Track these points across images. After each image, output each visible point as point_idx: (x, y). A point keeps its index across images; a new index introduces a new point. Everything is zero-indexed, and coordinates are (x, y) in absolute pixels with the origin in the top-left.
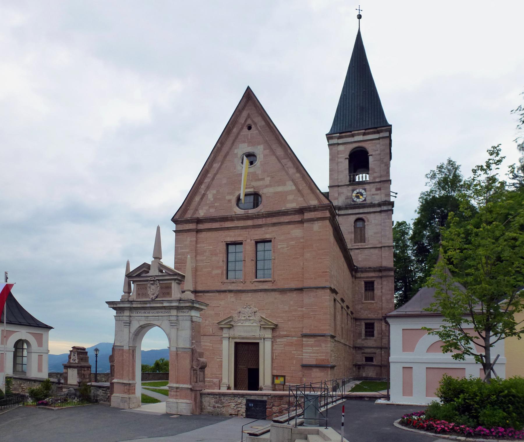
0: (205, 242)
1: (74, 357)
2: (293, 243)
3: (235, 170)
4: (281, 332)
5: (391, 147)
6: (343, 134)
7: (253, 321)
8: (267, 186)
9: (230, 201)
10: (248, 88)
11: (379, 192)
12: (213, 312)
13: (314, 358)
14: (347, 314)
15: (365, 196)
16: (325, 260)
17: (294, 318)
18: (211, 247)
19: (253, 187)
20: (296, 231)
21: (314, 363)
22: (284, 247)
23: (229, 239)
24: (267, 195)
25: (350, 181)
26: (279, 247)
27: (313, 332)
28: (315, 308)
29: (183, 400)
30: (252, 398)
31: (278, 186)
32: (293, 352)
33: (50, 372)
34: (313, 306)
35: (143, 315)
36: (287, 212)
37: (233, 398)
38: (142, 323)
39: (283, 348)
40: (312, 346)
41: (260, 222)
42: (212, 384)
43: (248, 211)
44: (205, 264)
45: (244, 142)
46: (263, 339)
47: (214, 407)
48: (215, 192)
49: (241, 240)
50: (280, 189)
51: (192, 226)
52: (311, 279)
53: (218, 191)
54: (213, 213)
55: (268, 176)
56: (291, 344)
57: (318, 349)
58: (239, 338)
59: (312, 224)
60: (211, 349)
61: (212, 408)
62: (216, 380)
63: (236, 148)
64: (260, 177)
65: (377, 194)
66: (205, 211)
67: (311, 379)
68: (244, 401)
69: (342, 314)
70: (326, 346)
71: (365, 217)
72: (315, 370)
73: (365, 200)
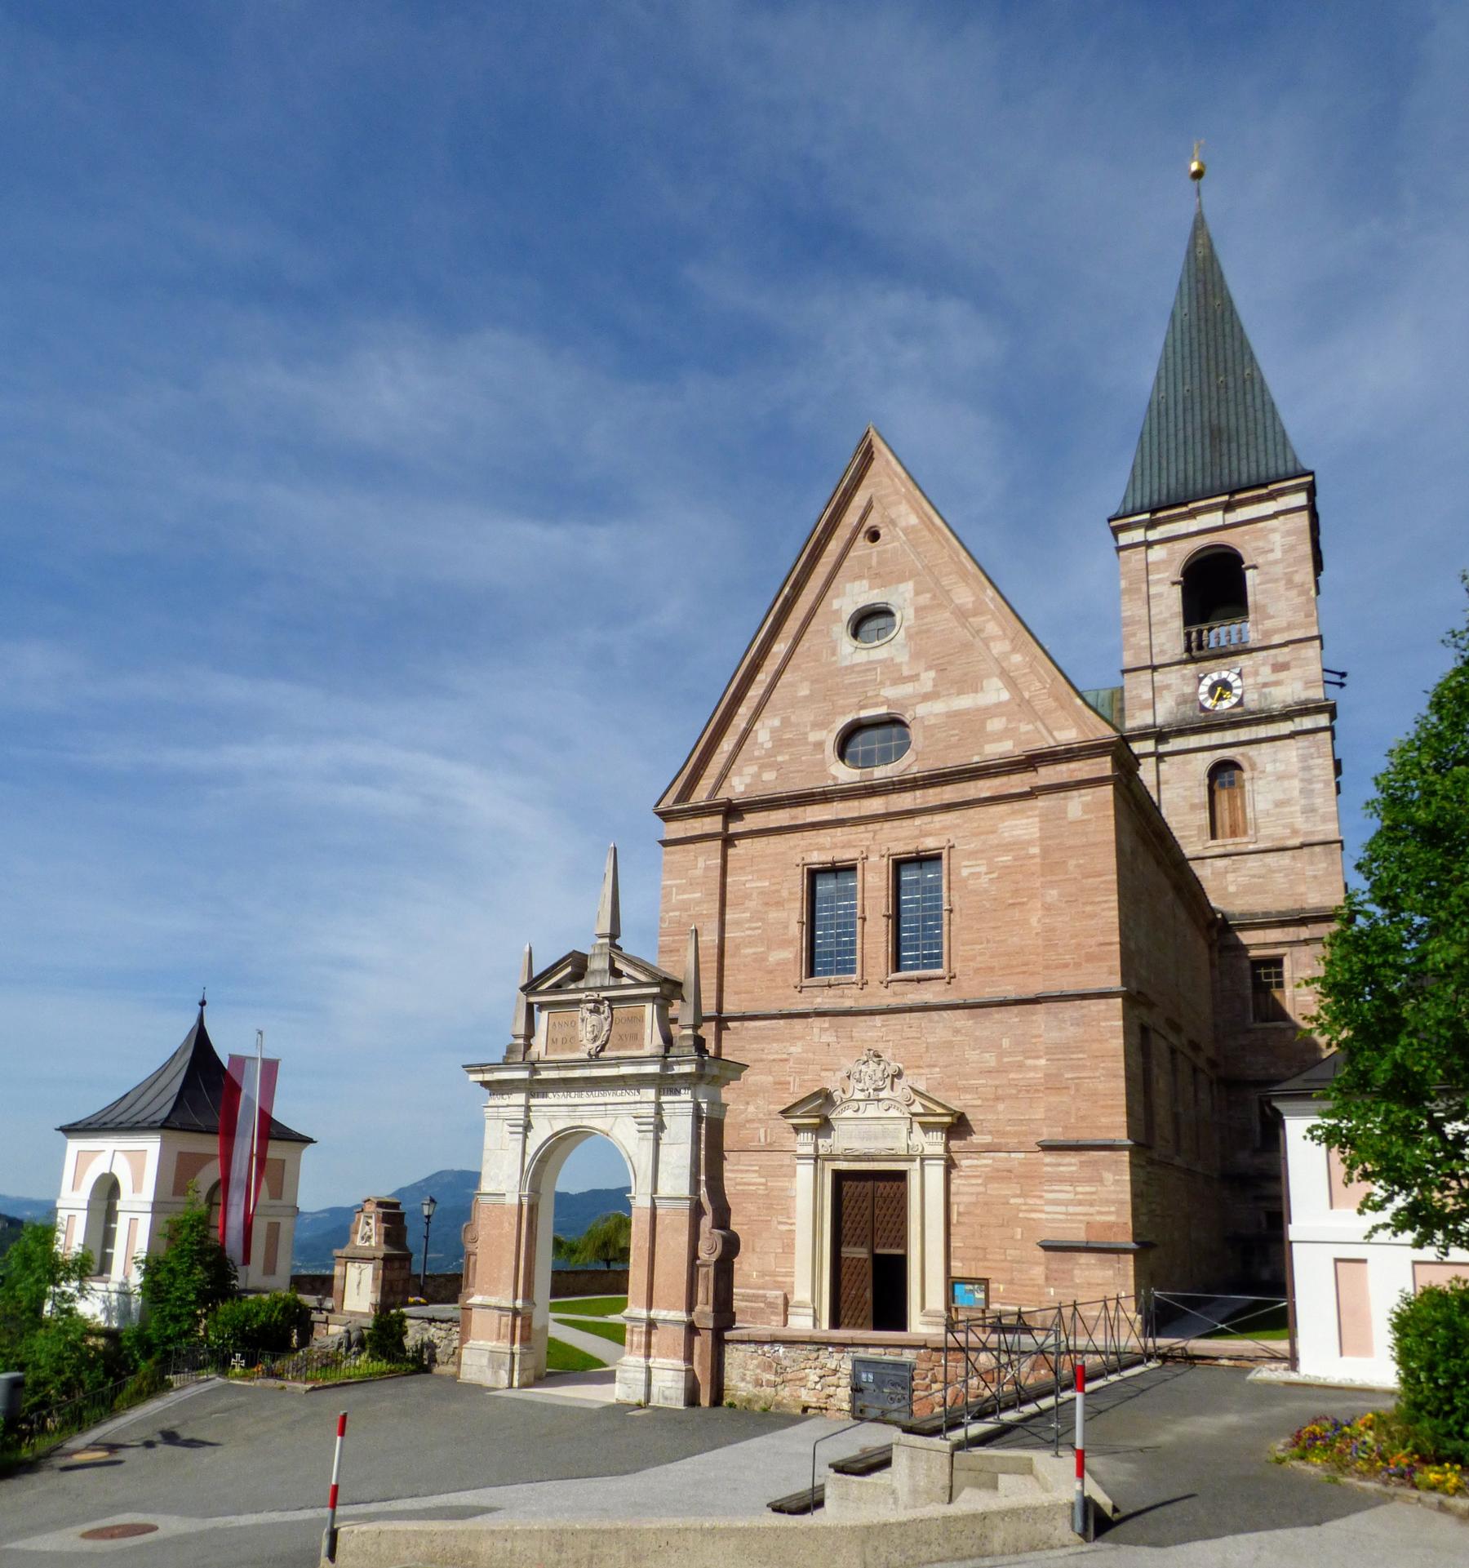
0: (748, 869)
1: (367, 1228)
2: (1006, 858)
3: (834, 659)
5: (1318, 533)
6: (1160, 515)
7: (887, 1102)
8: (926, 697)
9: (819, 745)
10: (660, 842)
11: (1283, 675)
12: (770, 1079)
13: (1081, 1221)
14: (1195, 1070)
15: (1238, 692)
16: (1106, 906)
17: (1014, 1092)
19: (888, 702)
20: (1014, 822)
21: (1079, 1236)
22: (979, 873)
23: (817, 858)
24: (926, 723)
25: (1188, 649)
26: (965, 872)
27: (1072, 1137)
28: (1079, 1059)
29: (665, 1361)
30: (872, 1353)
31: (959, 694)
32: (1012, 1201)
33: (294, 1273)
34: (1073, 1053)
35: (563, 1101)
36: (988, 767)
37: (815, 1355)
38: (559, 1125)
39: (981, 1189)
40: (1072, 1180)
41: (906, 801)
42: (762, 1305)
43: (872, 773)
44: (749, 932)
45: (860, 577)
46: (918, 1160)
47: (759, 1383)
48: (776, 722)
49: (852, 857)
50: (965, 702)
51: (713, 824)
52: (1066, 966)
53: (786, 722)
54: (771, 783)
55: (929, 668)
56: (1002, 1175)
57: (1093, 1189)
58: (847, 1158)
59: (1065, 799)
60: (760, 1192)
61: (750, 1386)
62: (775, 1295)
63: (837, 596)
64: (906, 672)
65: (1277, 683)
66: (748, 780)
67: (1071, 1290)
68: (847, 1366)
69: (1174, 1071)
70: (1118, 1181)
71: (1243, 755)
72: (1085, 1258)
73: (1240, 703)
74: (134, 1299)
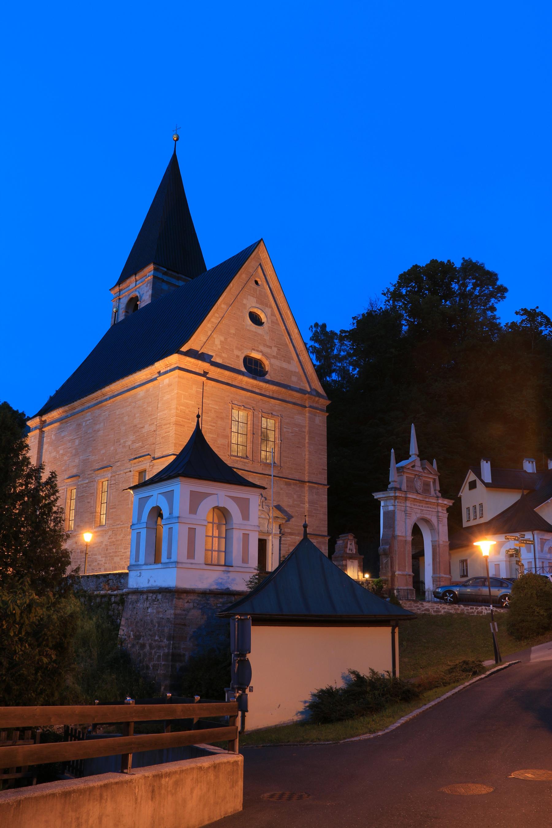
4: (285, 529)
6: (170, 272)
9: (238, 357)
17: (297, 515)
18: (217, 408)
52: (314, 474)
74: (397, 568)
